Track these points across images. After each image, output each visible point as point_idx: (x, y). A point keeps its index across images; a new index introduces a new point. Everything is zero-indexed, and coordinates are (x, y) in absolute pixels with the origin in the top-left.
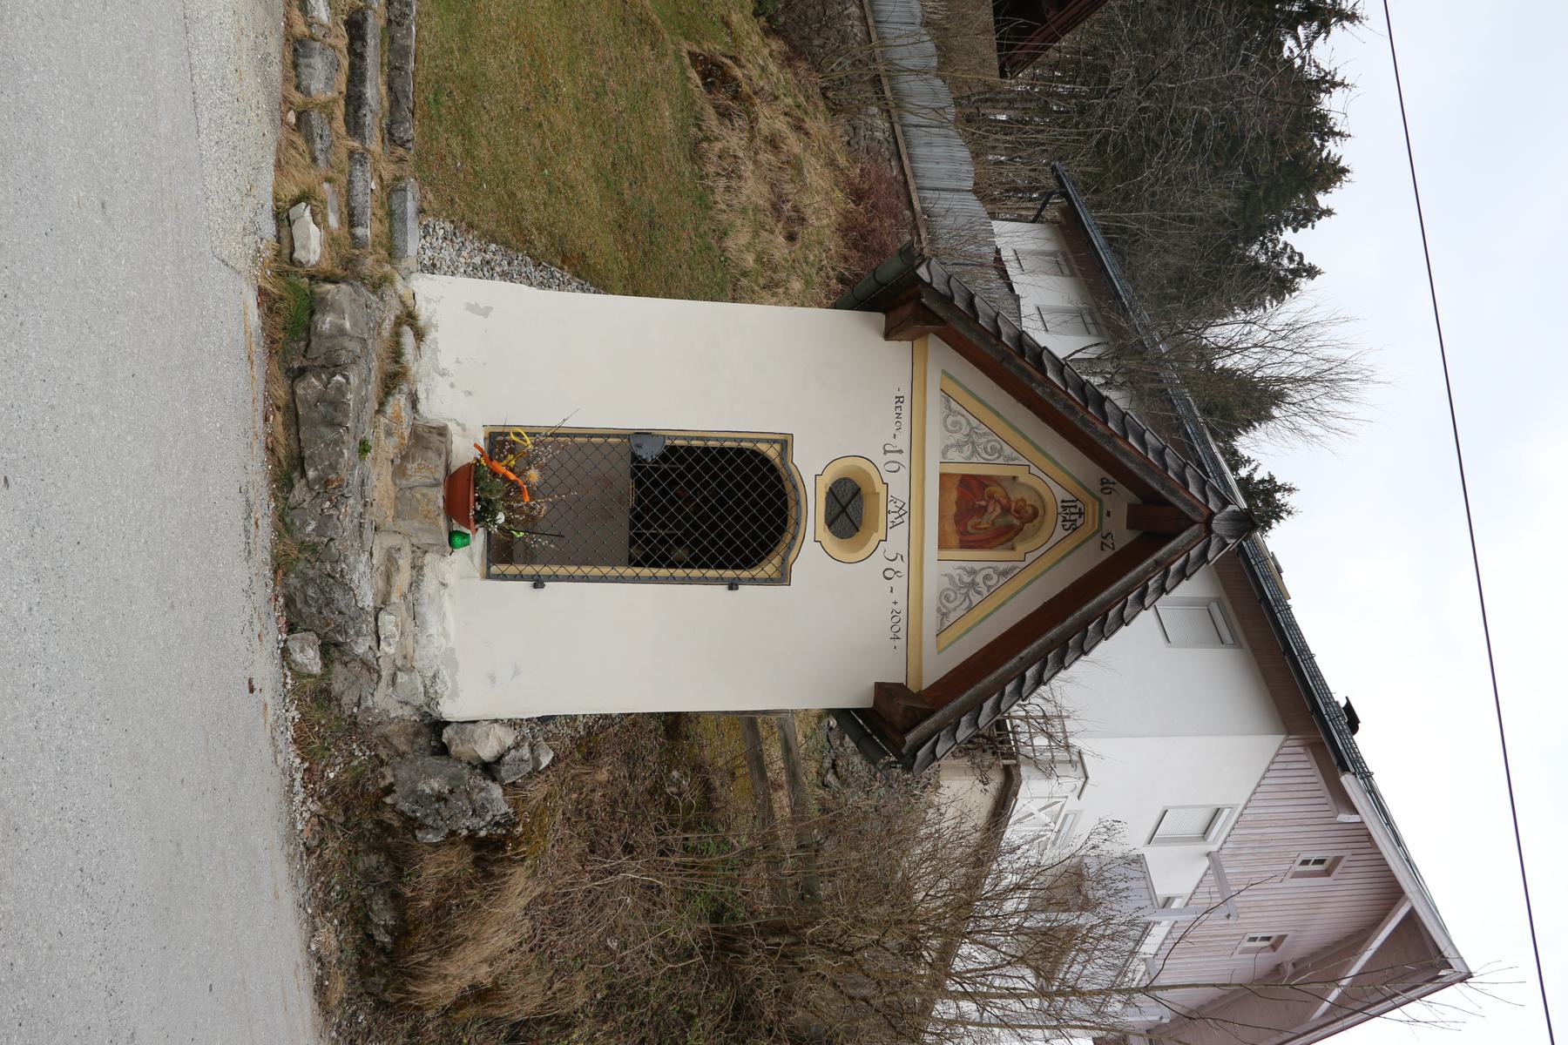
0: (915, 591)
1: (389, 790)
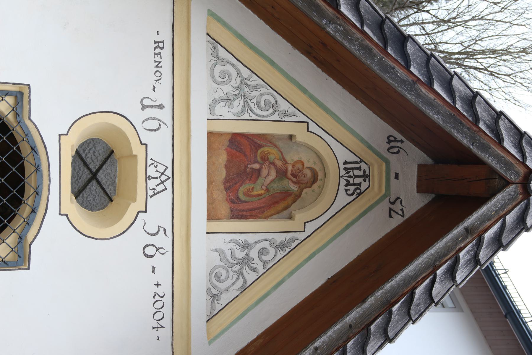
0: (181, 270)
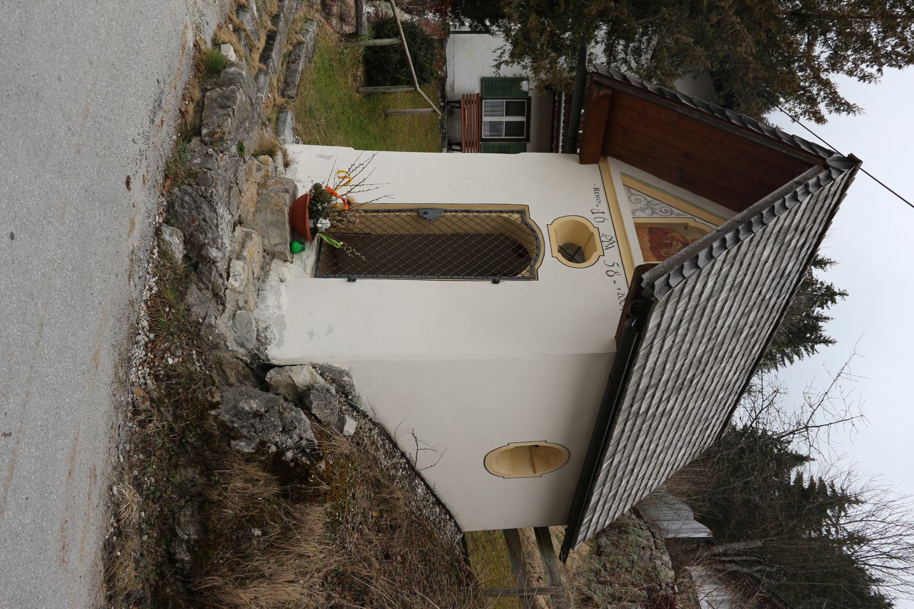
1: (215, 406)
